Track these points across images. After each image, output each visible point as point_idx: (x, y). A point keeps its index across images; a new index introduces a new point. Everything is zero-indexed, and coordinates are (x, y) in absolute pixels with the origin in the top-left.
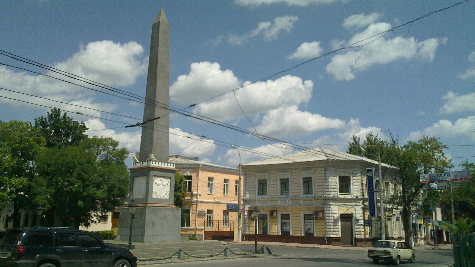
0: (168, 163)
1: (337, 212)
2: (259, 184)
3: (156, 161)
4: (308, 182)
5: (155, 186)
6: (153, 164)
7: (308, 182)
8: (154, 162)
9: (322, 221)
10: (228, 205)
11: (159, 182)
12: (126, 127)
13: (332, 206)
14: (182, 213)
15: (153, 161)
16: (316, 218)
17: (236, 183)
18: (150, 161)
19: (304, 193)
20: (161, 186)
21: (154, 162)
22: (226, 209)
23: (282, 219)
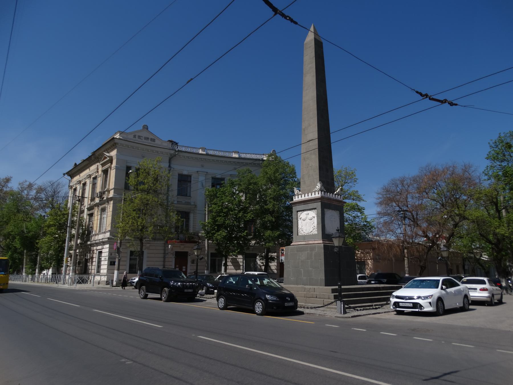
3: (325, 192)
5: (300, 222)
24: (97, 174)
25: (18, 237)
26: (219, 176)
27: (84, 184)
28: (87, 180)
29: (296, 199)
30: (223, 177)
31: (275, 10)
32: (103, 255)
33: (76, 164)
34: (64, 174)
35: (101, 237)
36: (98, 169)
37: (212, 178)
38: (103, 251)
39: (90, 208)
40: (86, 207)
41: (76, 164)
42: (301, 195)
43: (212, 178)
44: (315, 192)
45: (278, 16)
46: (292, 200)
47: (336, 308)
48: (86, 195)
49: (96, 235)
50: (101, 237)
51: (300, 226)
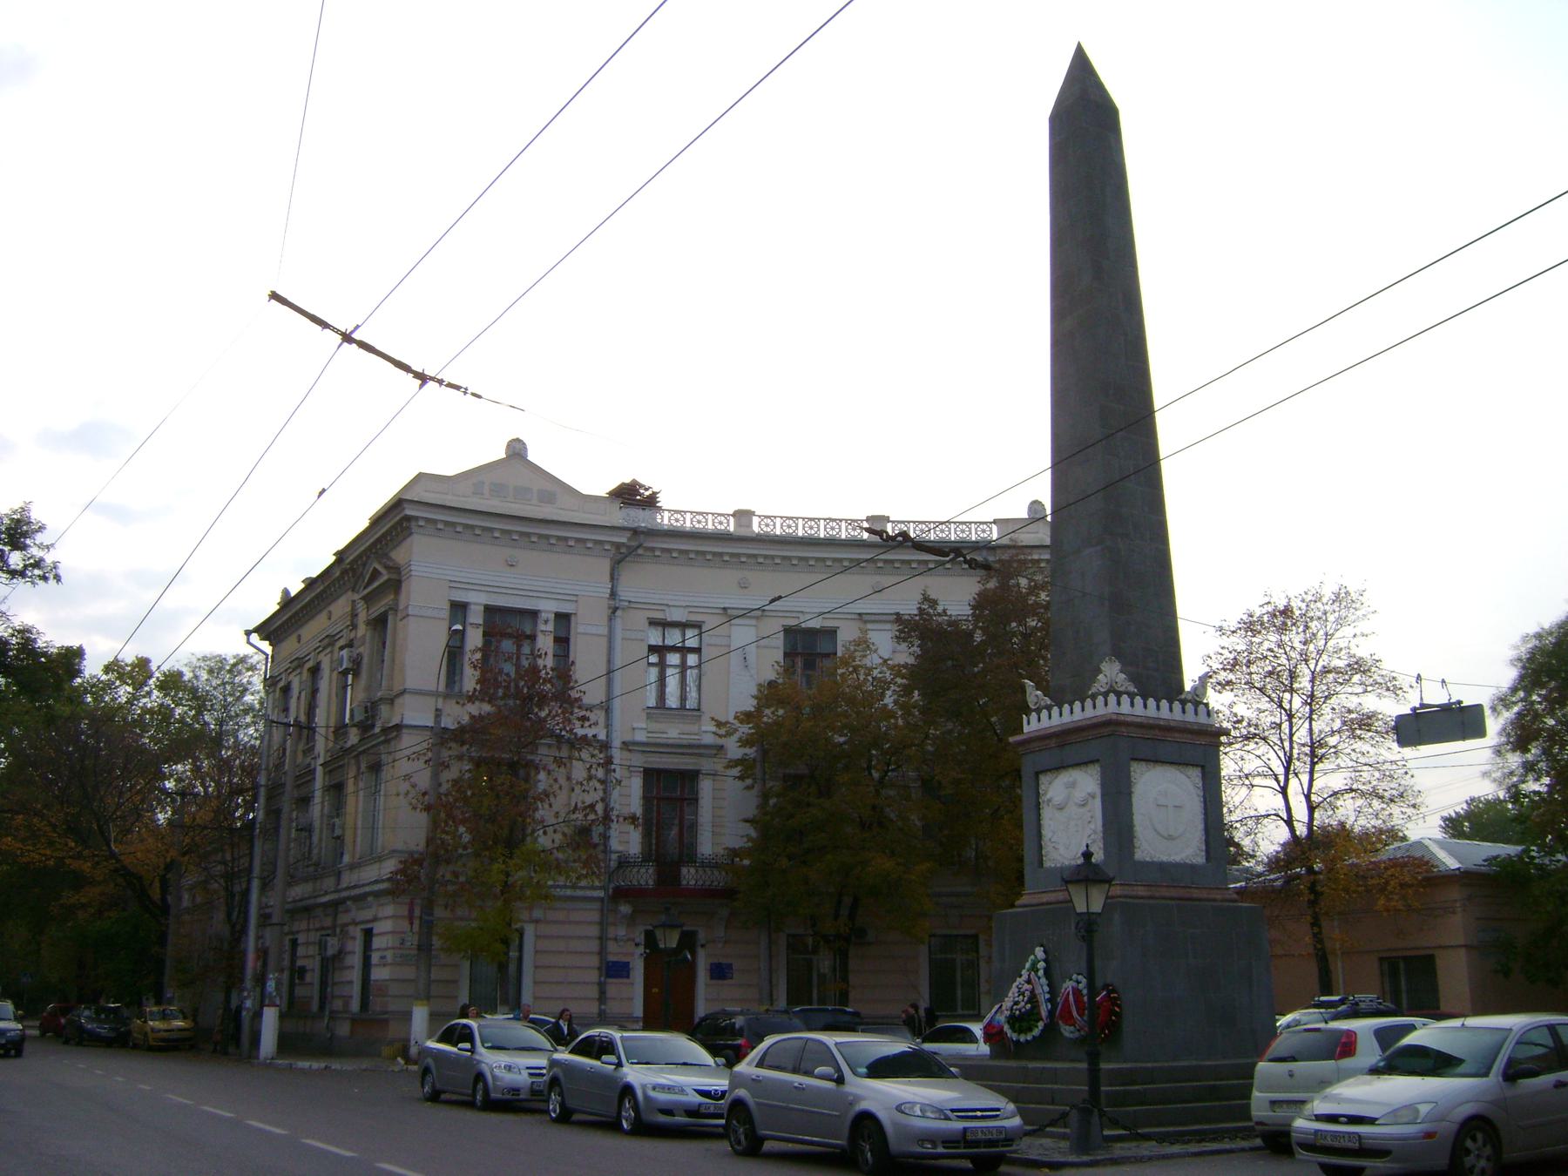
0: (1183, 703)
3: (1132, 696)
5: (1046, 813)
24: (352, 635)
25: (544, 841)
26: (815, 624)
27: (315, 671)
28: (321, 657)
29: (1032, 725)
30: (829, 624)
31: (423, 378)
32: (377, 942)
33: (286, 592)
34: (248, 633)
35: (370, 873)
36: (354, 615)
37: (788, 631)
38: (379, 927)
39: (333, 766)
40: (321, 761)
41: (286, 592)
42: (1049, 708)
43: (788, 631)
44: (1094, 697)
45: (431, 384)
46: (1019, 729)
47: (1063, 1137)
48: (320, 718)
49: (353, 867)
50: (370, 873)
51: (1046, 833)
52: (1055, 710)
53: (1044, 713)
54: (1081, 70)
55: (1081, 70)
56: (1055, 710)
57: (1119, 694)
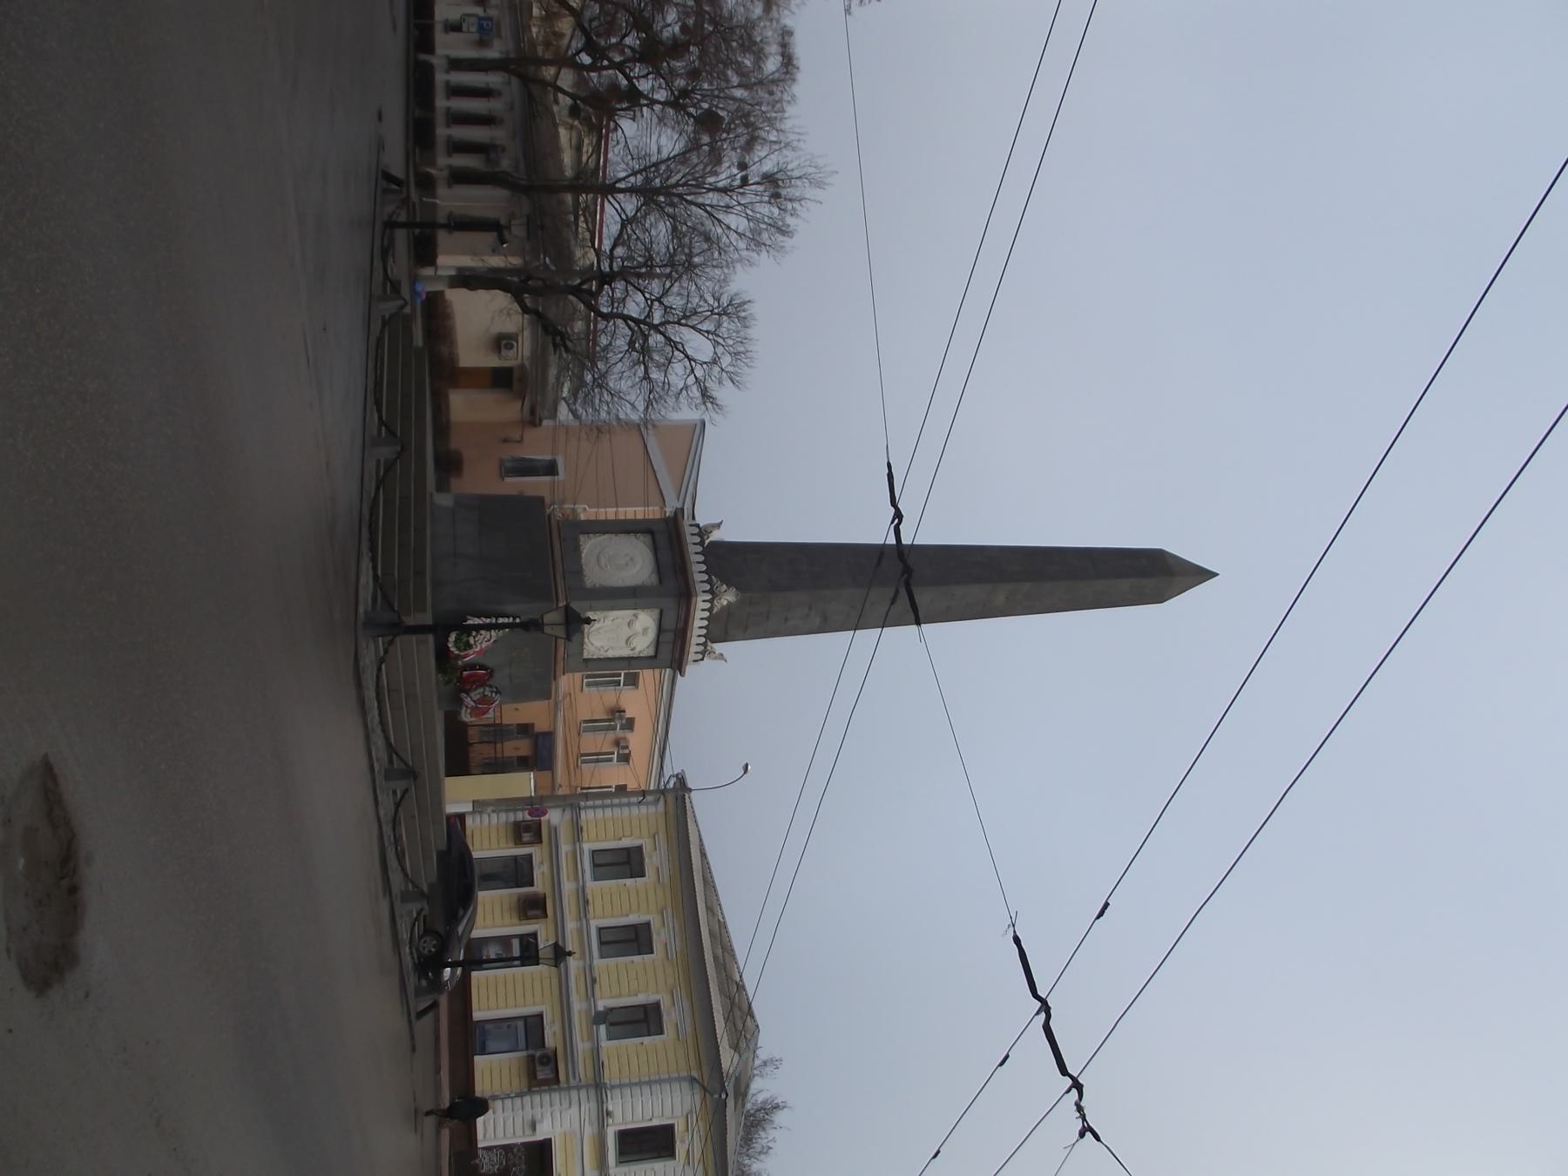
0: (705, 644)
1: (558, 1129)
2: (634, 928)
3: (710, 610)
4: (644, 1020)
5: (628, 613)
6: (701, 604)
7: (644, 1020)
8: (708, 605)
9: (525, 1082)
10: (549, 736)
11: (638, 626)
12: (1017, 940)
13: (575, 1109)
14: (465, 771)
15: (711, 601)
16: (531, 1059)
17: (618, 787)
18: (711, 591)
19: (600, 930)
20: (626, 632)
21: (708, 605)
22: (537, 729)
23: (521, 937)
52: (700, 549)
53: (698, 540)
54: (1203, 575)
55: (1203, 575)
56: (700, 549)
57: (711, 601)
